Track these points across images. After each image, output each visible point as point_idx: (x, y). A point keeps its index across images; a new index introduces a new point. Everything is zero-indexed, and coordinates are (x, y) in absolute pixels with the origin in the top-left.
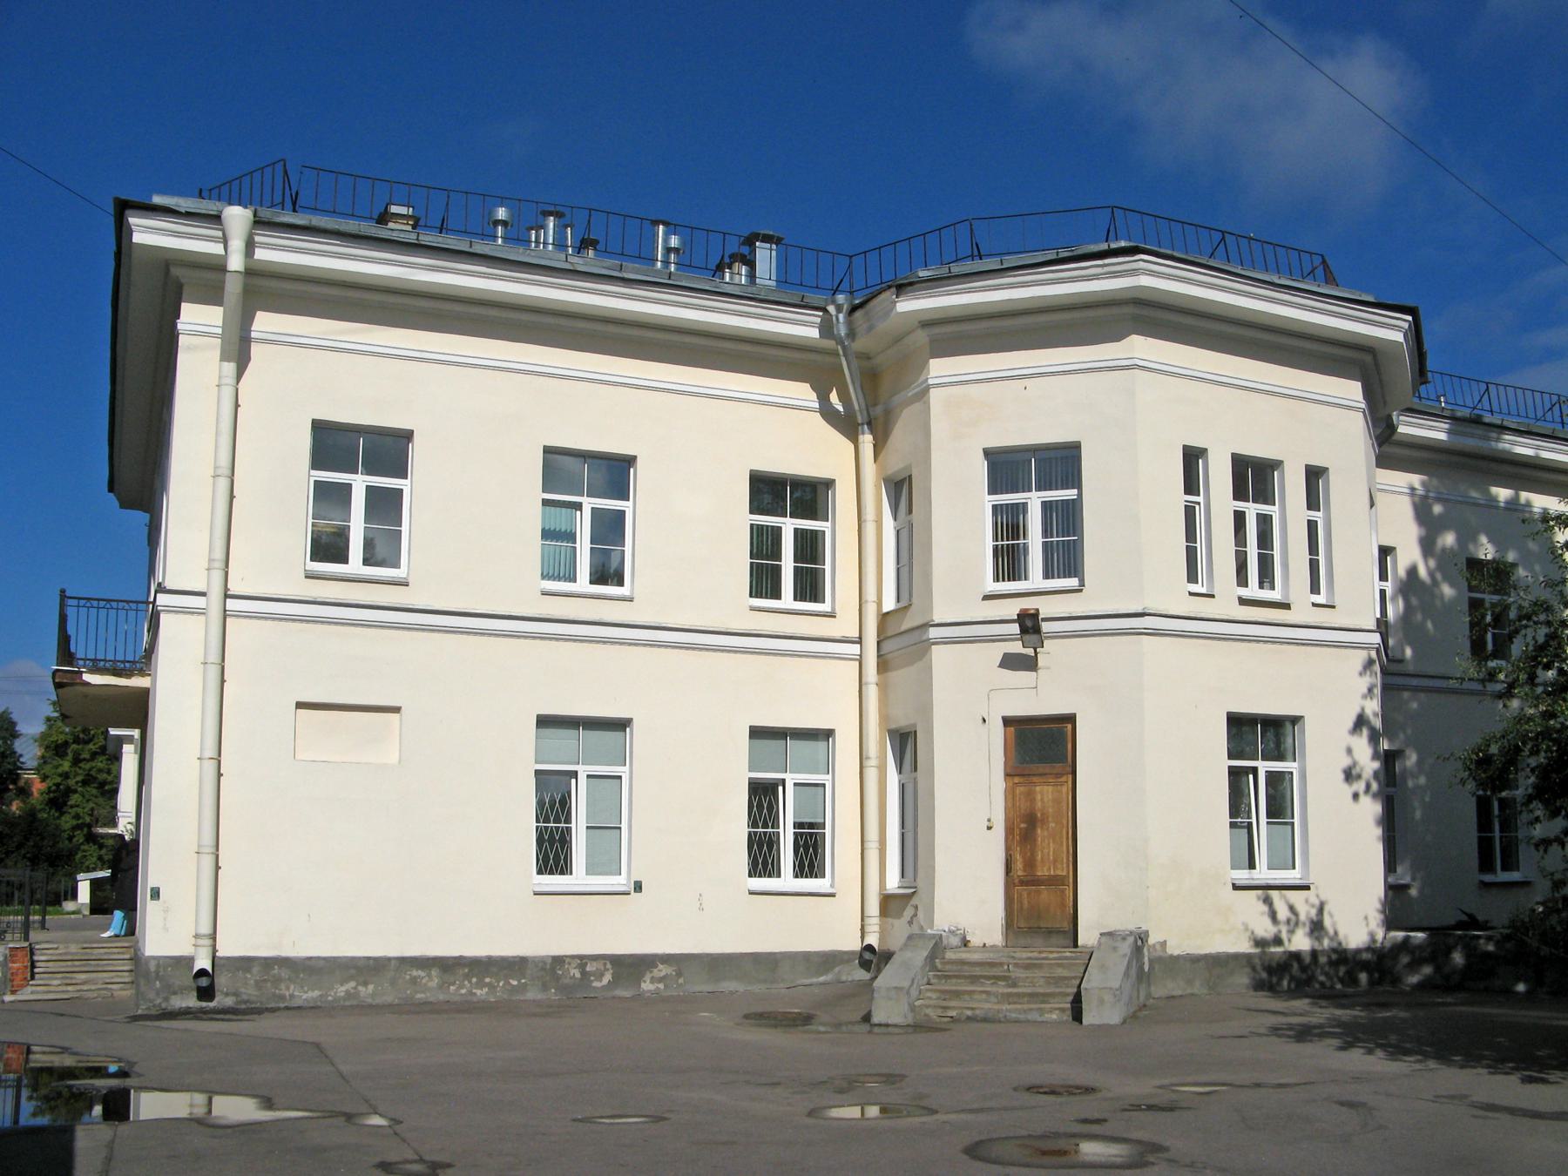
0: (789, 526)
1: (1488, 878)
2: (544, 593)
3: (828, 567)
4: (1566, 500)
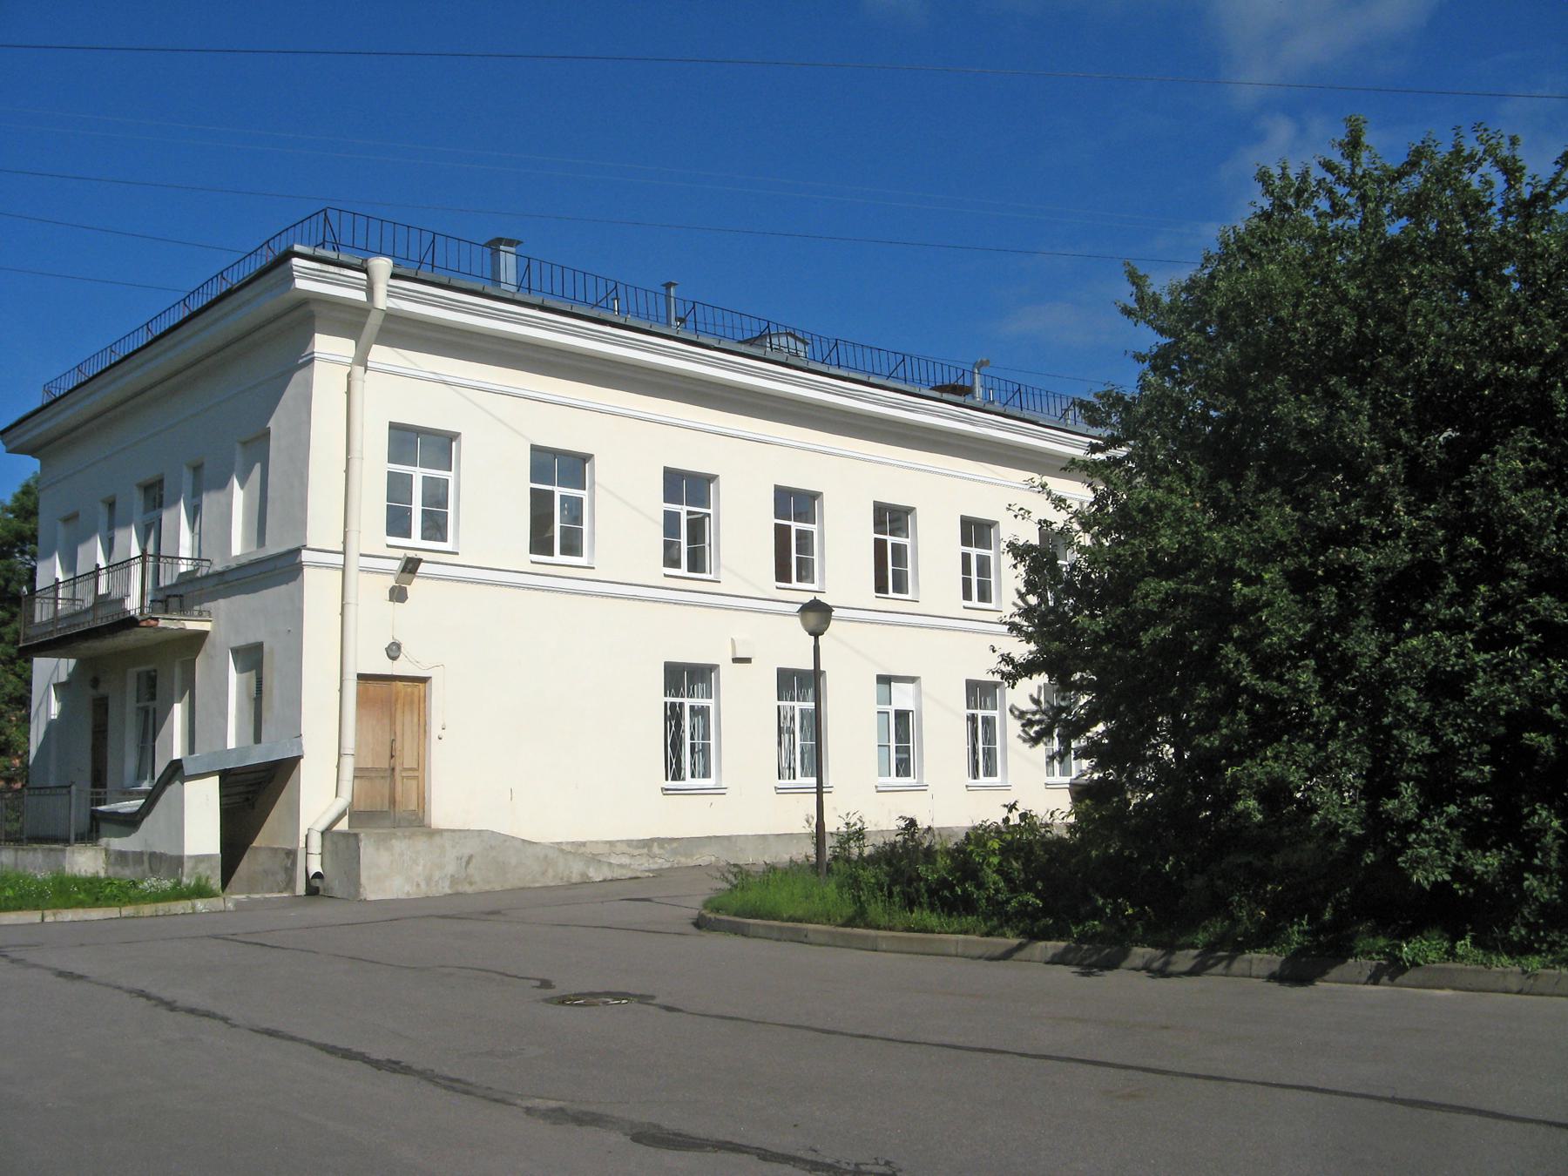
0: (418, 474)
1: (1051, 780)
2: (965, 608)
3: (909, 569)
4: (1566, 605)
